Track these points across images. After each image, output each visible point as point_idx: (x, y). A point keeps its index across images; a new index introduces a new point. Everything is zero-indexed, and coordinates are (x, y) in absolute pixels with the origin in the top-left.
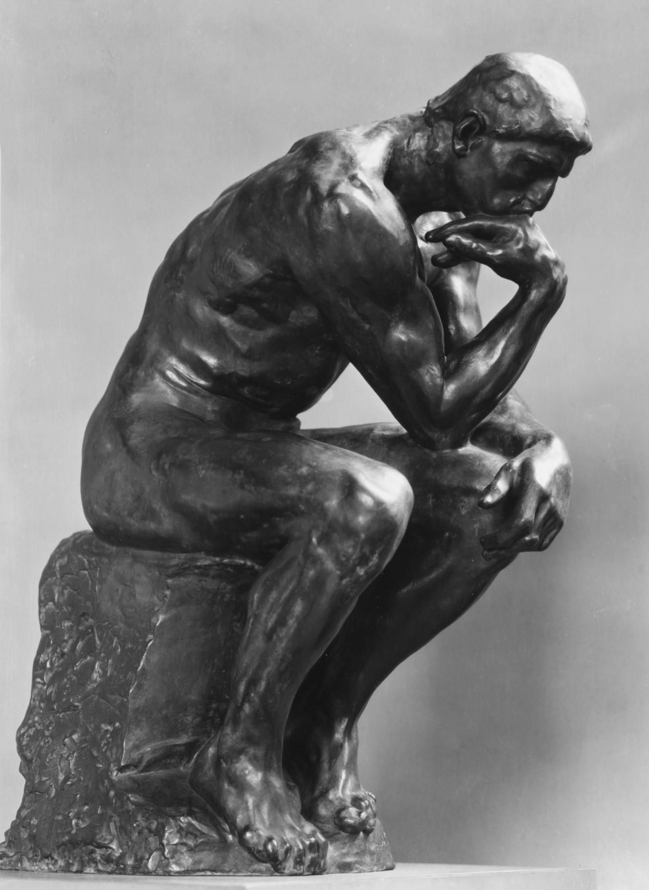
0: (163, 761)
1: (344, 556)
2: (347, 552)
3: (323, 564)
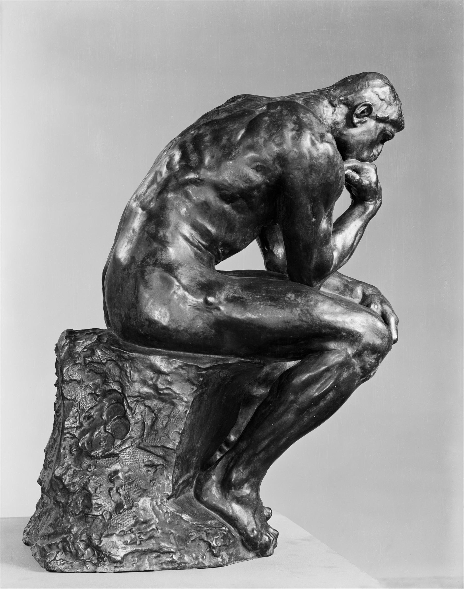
1: (369, 365)
2: (371, 362)
3: (354, 368)
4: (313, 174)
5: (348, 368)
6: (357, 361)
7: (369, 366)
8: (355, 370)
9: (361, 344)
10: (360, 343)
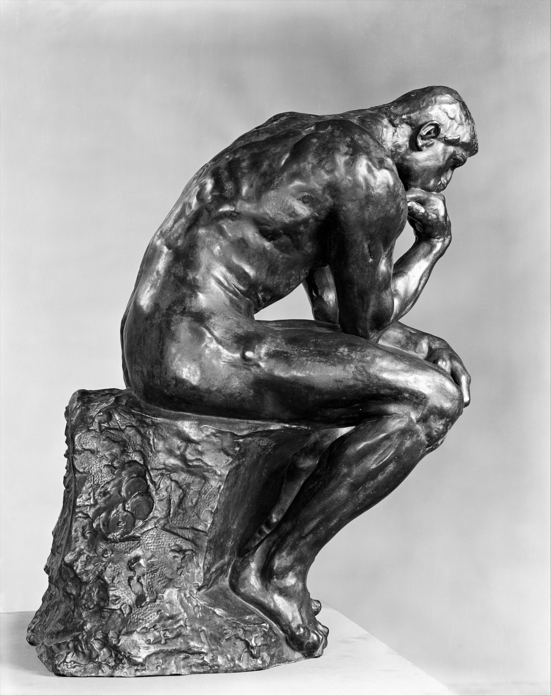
0: (365, 149)
1: (436, 431)
2: (439, 429)
3: (418, 436)
4: (370, 206)
5: (412, 436)
6: (422, 427)
7: (435, 433)
8: (419, 438)
9: (427, 407)
10: (425, 406)
